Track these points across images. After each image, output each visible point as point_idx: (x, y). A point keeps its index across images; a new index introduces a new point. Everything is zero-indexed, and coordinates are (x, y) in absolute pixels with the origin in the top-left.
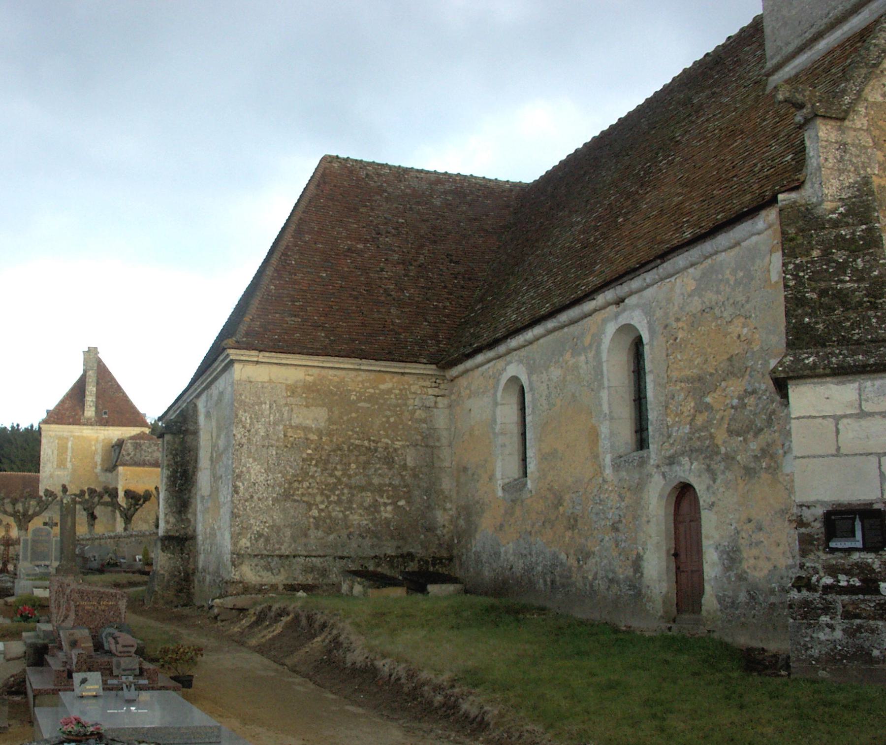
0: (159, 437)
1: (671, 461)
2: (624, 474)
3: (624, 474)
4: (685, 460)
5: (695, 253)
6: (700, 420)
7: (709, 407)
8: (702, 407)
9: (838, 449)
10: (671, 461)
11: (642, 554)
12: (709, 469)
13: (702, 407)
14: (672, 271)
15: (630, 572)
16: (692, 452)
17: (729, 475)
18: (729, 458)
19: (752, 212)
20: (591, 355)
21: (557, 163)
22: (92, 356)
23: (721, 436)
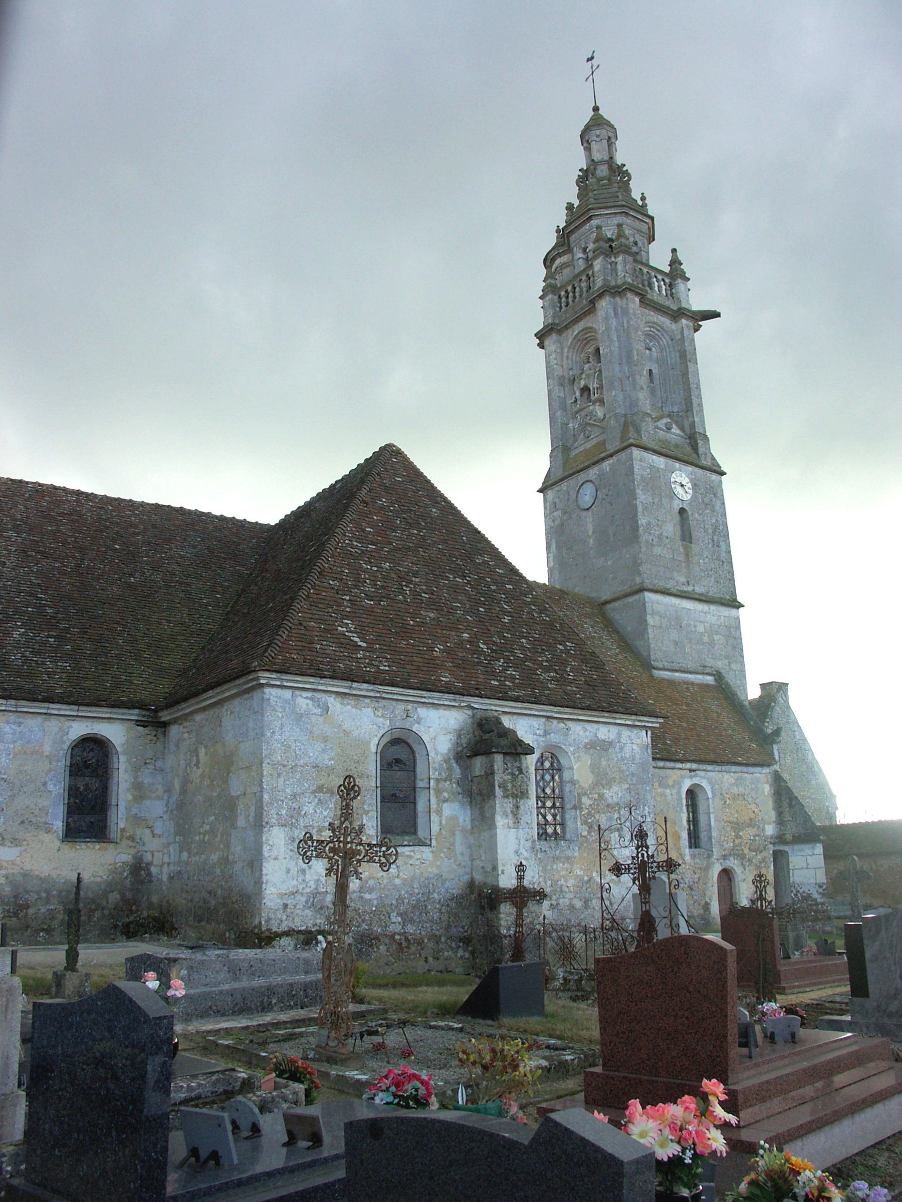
0: (330, 824)
1: (725, 857)
2: (697, 860)
3: (697, 860)
4: (732, 858)
5: (739, 768)
6: (737, 842)
7: (741, 837)
8: (738, 836)
9: (808, 864)
10: (725, 857)
11: (709, 901)
12: (742, 864)
13: (738, 836)
14: (727, 770)
15: (702, 911)
16: (736, 856)
17: (751, 868)
18: (749, 860)
19: (762, 765)
20: (674, 791)
21: (302, 504)
22: (743, 606)
23: (746, 851)
